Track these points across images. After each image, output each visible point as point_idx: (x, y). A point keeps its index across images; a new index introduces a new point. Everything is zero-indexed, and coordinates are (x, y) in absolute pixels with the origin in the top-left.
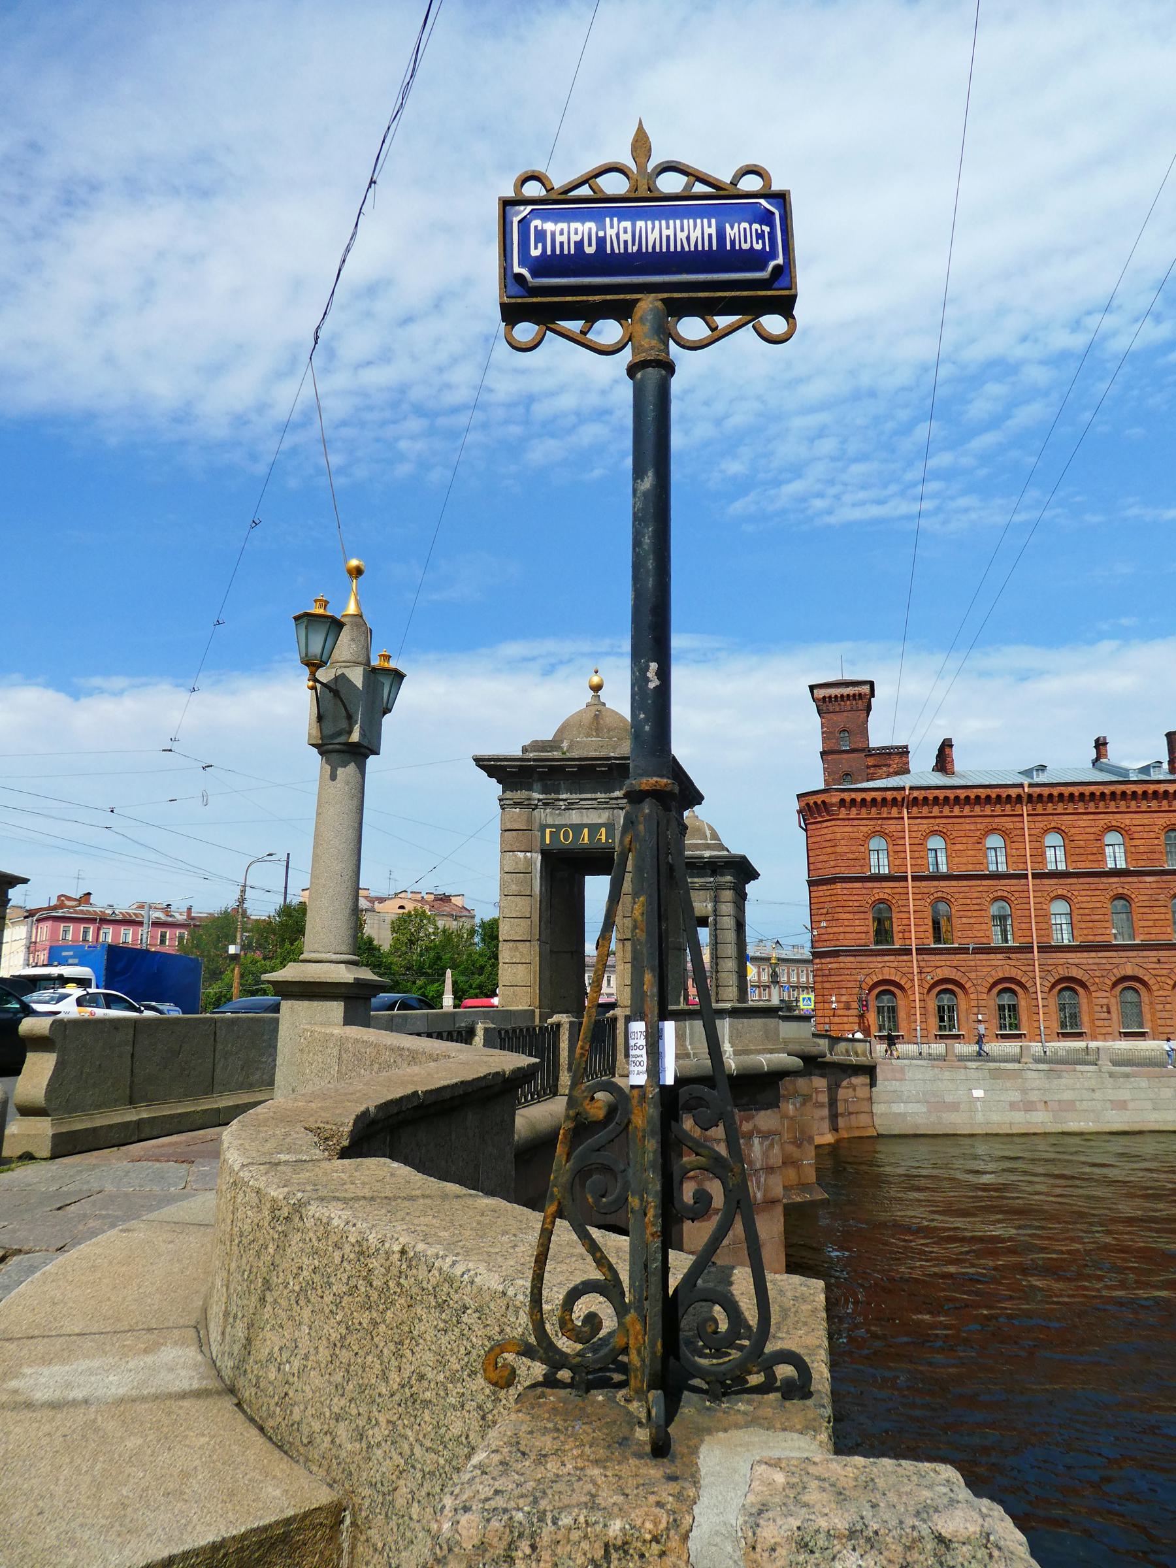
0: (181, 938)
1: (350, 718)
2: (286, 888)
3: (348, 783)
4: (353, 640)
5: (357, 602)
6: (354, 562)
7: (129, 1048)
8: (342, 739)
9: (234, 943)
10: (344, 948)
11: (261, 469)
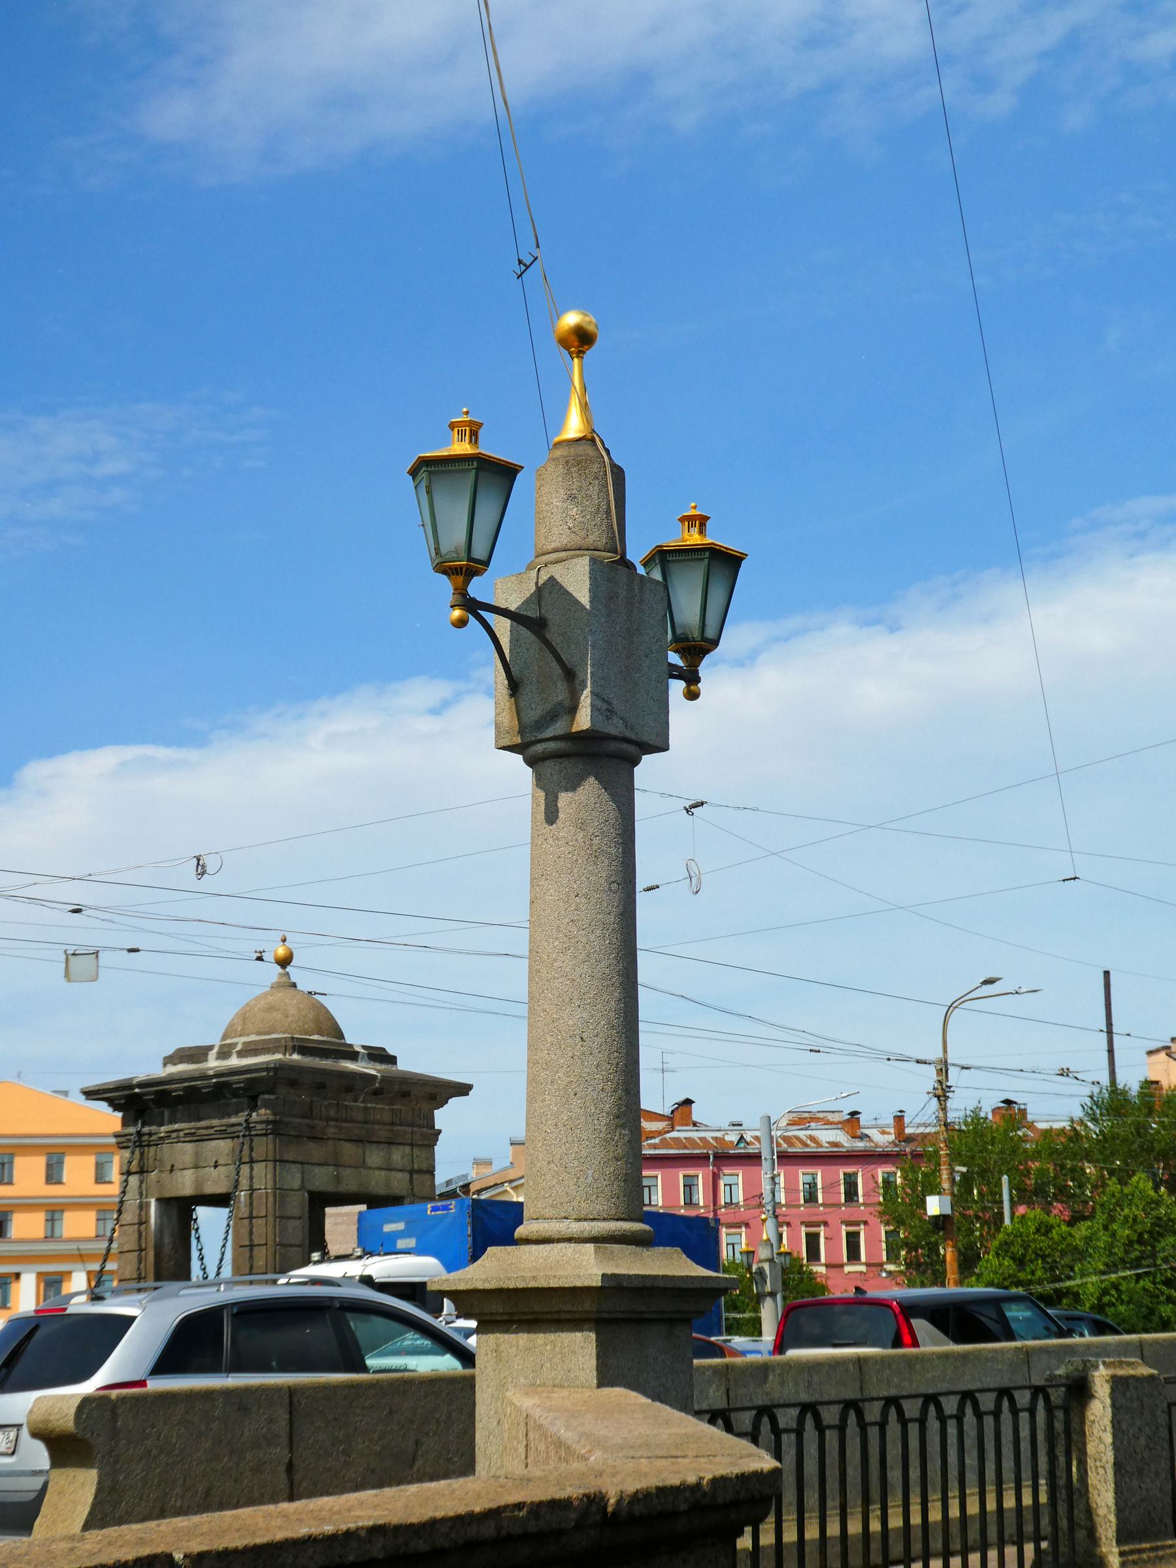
0: (888, 1183)
1: (570, 675)
2: (1111, 1051)
3: (582, 826)
4: (572, 497)
5: (585, 407)
6: (571, 319)
7: (280, 1452)
8: (558, 728)
9: (935, 1189)
10: (601, 1206)
11: (1000, 103)
